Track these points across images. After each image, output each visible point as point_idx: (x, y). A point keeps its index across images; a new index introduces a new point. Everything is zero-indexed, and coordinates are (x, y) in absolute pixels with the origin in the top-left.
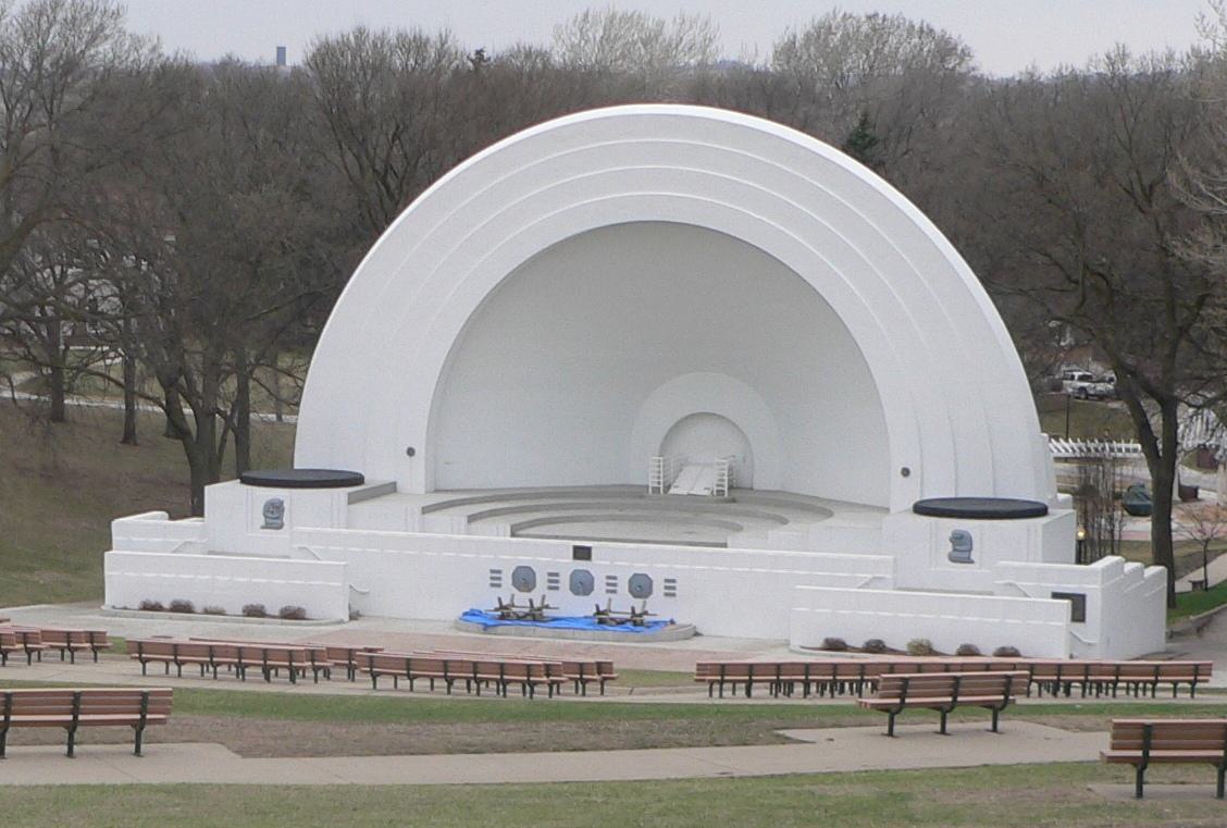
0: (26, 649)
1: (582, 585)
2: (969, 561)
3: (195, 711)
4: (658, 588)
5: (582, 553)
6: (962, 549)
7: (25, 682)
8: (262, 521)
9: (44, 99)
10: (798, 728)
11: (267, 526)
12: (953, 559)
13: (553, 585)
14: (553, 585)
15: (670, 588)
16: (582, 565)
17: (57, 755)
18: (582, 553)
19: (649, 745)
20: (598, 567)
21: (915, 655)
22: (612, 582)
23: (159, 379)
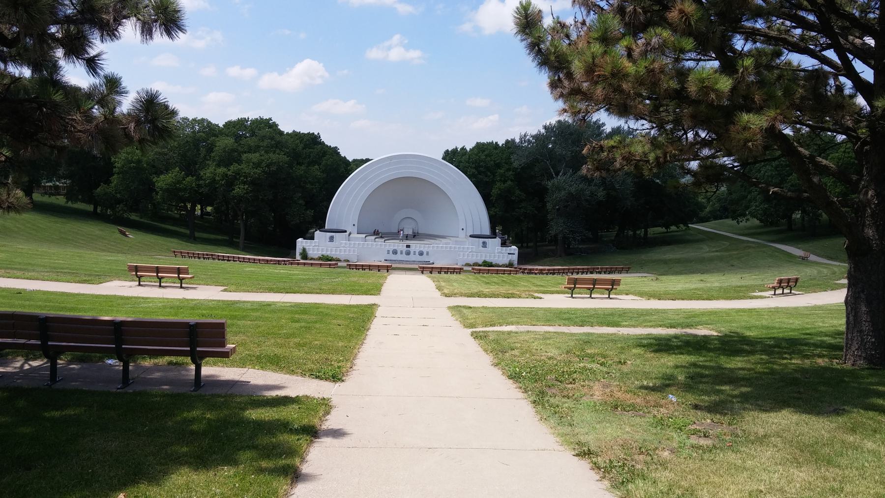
0: (136, 274)
1: (408, 253)
2: (486, 247)
3: (851, 413)
4: (425, 253)
5: (408, 246)
6: (484, 245)
7: (403, 272)
8: (329, 240)
9: (134, 304)
10: (306, 293)
11: (330, 241)
12: (483, 247)
13: (401, 253)
14: (401, 253)
15: (428, 253)
16: (408, 249)
17: (178, 287)
18: (408, 246)
19: (705, 296)
20: (412, 249)
21: (484, 266)
22: (415, 253)
23: (787, 20)
